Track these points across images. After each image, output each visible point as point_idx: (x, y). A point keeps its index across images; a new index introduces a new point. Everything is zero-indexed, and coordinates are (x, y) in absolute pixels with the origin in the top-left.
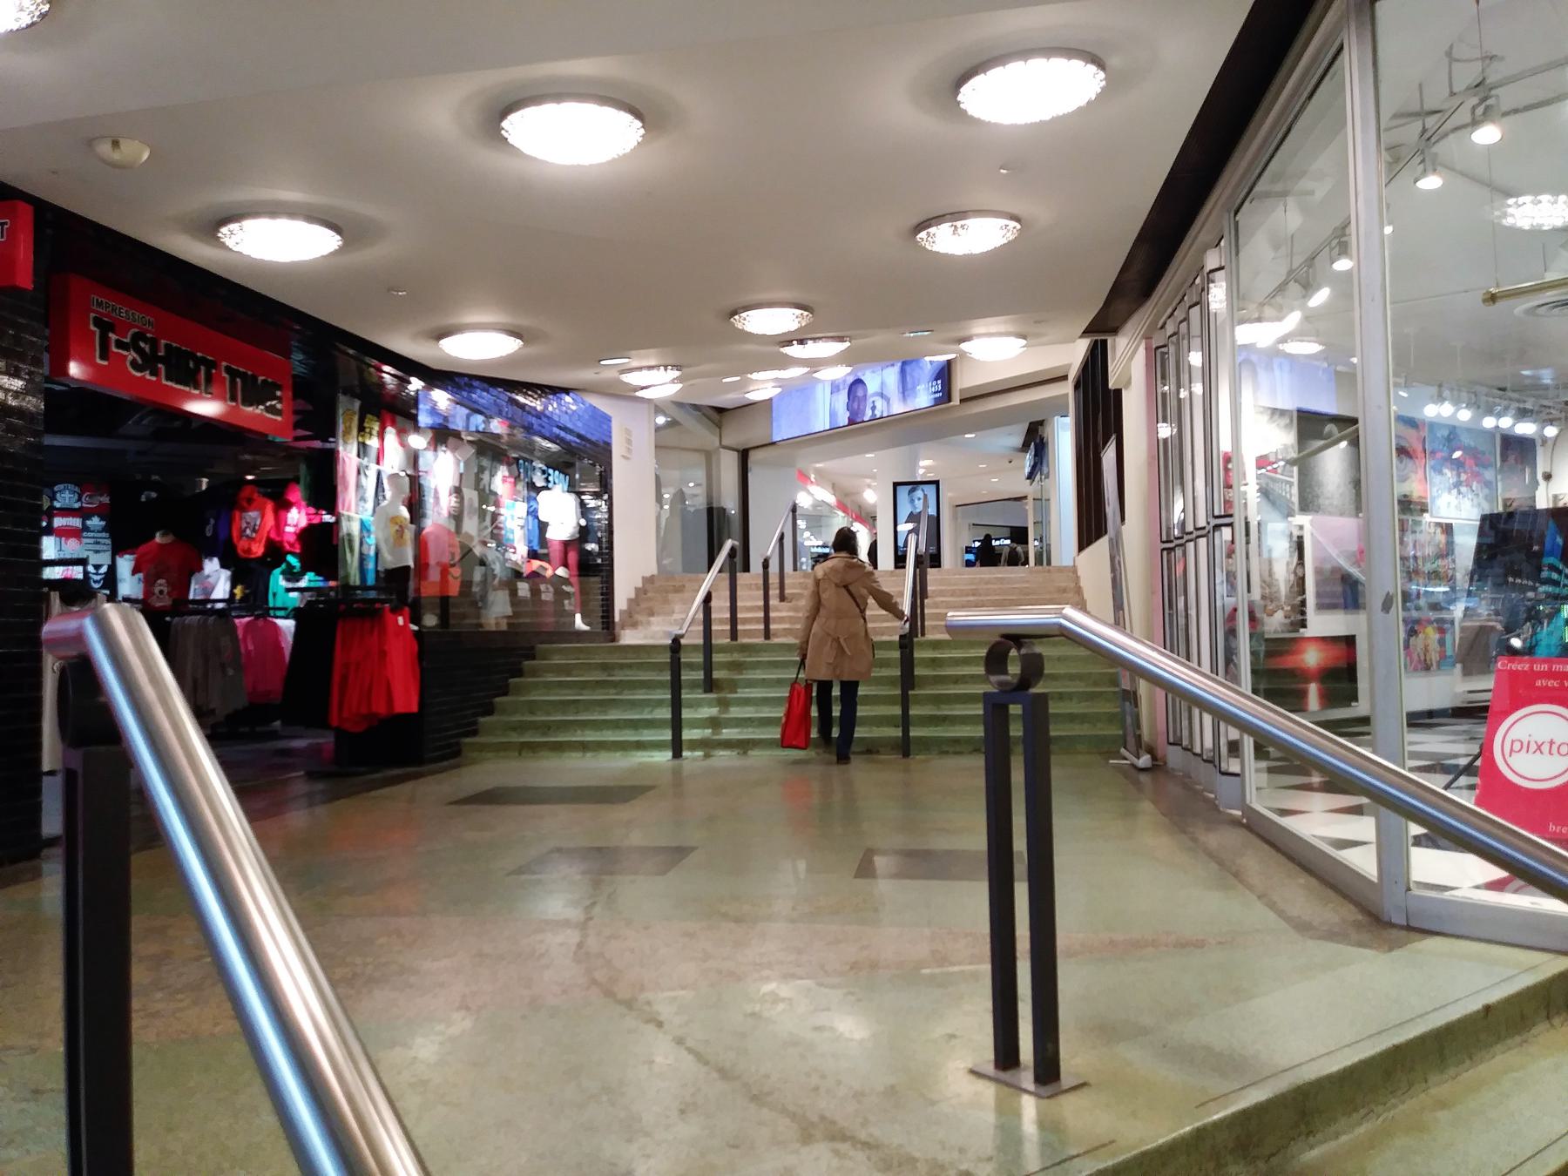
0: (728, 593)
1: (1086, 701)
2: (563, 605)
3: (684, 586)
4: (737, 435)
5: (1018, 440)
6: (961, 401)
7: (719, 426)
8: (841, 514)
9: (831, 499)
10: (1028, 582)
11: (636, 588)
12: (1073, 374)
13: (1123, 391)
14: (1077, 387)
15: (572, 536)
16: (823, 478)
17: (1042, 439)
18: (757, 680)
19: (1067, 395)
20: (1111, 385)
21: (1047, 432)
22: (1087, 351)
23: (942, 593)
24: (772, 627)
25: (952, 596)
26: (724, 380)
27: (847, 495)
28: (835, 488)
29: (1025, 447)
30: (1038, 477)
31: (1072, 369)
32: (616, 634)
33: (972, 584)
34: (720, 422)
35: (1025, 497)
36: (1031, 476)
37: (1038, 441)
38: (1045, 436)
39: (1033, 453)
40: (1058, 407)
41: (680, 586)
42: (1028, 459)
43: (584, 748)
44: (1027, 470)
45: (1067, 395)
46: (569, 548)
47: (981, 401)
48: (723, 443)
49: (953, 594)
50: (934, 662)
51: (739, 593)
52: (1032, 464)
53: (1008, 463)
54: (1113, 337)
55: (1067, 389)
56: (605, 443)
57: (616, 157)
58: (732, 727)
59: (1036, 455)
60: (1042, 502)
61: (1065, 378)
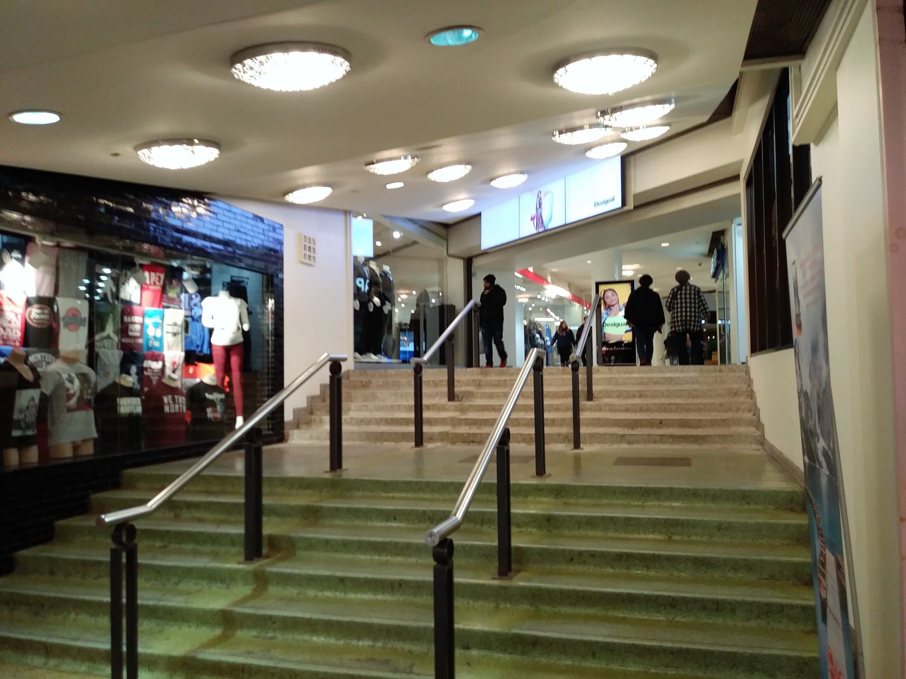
0: (412, 391)
1: (758, 617)
2: (206, 413)
3: (370, 382)
4: (460, 245)
5: (704, 248)
6: (634, 208)
7: (446, 239)
8: (577, 305)
9: (566, 294)
10: (697, 382)
11: (321, 386)
12: (743, 173)
13: (812, 146)
14: (748, 184)
15: (233, 340)
16: (558, 279)
17: (723, 246)
18: (318, 541)
19: (738, 195)
20: (793, 139)
21: (726, 240)
22: (759, 135)
23: (608, 394)
24: (426, 429)
25: (618, 397)
26: (21, 118)
27: (582, 291)
28: (570, 286)
29: (710, 253)
30: (721, 276)
31: (744, 164)
32: (285, 434)
33: (640, 384)
34: (447, 235)
35: (714, 291)
36: (715, 275)
37: (720, 247)
38: (726, 243)
39: (716, 257)
40: (727, 209)
41: (366, 383)
42: (713, 262)
43: (48, 653)
44: (712, 271)
45: (738, 195)
46: (231, 353)
47: (651, 208)
48: (450, 252)
49: (619, 395)
50: (548, 522)
51: (425, 390)
52: (715, 265)
53: (698, 264)
54: (798, 62)
55: (739, 188)
56: (276, 251)
57: (562, 143)
58: (249, 627)
59: (718, 259)
60: (724, 294)
61: (736, 178)
